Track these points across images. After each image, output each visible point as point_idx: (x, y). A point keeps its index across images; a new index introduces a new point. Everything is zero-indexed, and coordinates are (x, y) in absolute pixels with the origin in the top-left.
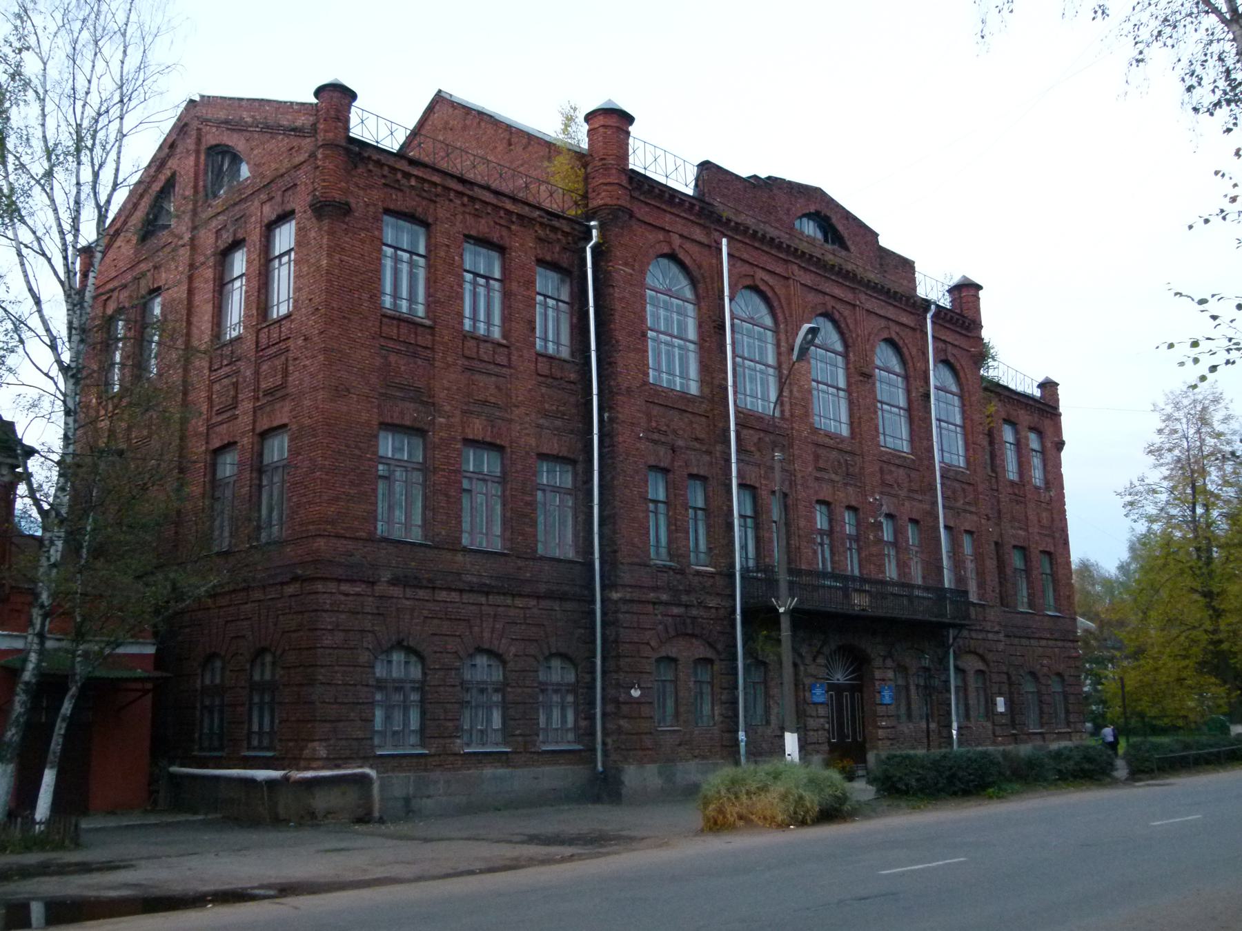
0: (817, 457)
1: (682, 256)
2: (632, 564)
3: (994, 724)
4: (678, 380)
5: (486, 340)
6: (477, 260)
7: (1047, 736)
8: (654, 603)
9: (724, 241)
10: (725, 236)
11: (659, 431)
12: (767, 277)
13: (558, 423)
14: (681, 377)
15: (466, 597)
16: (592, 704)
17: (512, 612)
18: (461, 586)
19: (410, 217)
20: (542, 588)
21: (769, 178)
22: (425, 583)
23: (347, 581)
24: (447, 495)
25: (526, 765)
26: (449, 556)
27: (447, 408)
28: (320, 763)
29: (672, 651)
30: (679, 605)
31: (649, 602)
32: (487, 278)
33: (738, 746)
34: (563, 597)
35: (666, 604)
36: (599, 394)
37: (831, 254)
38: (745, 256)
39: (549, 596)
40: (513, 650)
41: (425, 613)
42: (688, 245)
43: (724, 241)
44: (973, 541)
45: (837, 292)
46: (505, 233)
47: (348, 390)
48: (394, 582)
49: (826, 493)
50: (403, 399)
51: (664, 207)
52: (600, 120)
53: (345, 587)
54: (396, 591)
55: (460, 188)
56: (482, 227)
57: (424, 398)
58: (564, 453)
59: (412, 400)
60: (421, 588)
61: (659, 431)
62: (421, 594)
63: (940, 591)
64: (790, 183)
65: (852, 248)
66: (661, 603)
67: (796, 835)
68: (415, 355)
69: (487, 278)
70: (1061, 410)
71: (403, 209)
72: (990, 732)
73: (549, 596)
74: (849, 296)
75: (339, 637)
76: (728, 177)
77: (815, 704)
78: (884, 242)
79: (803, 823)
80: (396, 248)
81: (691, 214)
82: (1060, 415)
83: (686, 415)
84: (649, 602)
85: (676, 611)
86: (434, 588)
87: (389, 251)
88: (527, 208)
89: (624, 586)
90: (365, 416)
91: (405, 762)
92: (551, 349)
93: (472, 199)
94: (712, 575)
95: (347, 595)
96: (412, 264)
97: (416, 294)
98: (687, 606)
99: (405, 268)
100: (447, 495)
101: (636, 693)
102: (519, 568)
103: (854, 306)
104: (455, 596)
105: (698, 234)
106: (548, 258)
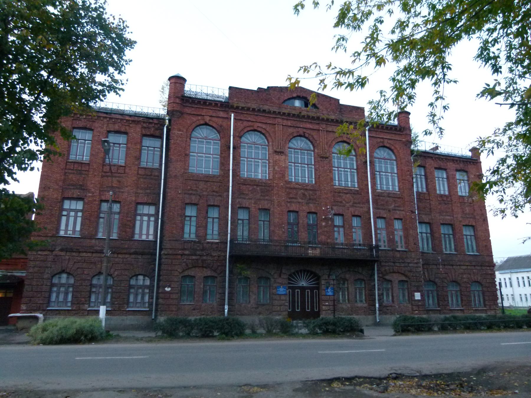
0: (289, 193)
1: (211, 123)
2: (170, 240)
3: (412, 305)
4: (343, 182)
5: (445, 196)
6: (458, 175)
7: (465, 311)
8: (182, 255)
9: (233, 115)
10: (233, 112)
11: (192, 190)
12: (260, 125)
13: (148, 191)
14: (345, 181)
15: (94, 255)
16: (153, 293)
17: (117, 260)
18: (92, 251)
19: (85, 128)
20: (132, 251)
21: (268, 87)
22: (74, 250)
23: (85, 252)
24: (90, 220)
25: (118, 315)
26: (88, 241)
27: (93, 190)
28: (23, 312)
29: (191, 273)
30: (196, 255)
31: (179, 255)
32: (463, 180)
33: (224, 311)
34: (142, 254)
35: (188, 255)
36: (164, 179)
37: (310, 111)
38: (249, 119)
39: (136, 253)
40: (116, 273)
41: (75, 260)
42: (214, 119)
43: (233, 115)
44: (402, 222)
45: (311, 126)
46: (127, 128)
47: (49, 188)
48: (62, 250)
49: (293, 207)
50: (73, 189)
51: (202, 107)
52: (173, 81)
53: (39, 253)
54: (63, 253)
55: (105, 115)
56: (458, 167)
57: (83, 188)
58: (150, 201)
59: (77, 188)
60: (74, 252)
61: (192, 190)
62: (74, 254)
63: (371, 248)
64: (281, 87)
65: (321, 107)
66: (185, 255)
67: (42, 347)
68: (81, 174)
69: (463, 180)
70: (481, 160)
71: (81, 126)
72: (410, 309)
73: (136, 253)
74: (316, 127)
75: (36, 269)
76: (237, 91)
77: (279, 294)
78: (341, 102)
79: (44, 344)
80: (380, 172)
81: (218, 107)
82: (481, 162)
83: (208, 183)
84: (179, 255)
85: (194, 257)
86: (80, 252)
87: (378, 173)
88: (136, 118)
89: (166, 249)
90: (55, 196)
91: (61, 312)
92: (442, 193)
93: (111, 118)
94: (217, 243)
95: (42, 255)
96: (421, 178)
97: (395, 184)
98: (200, 256)
99: (419, 179)
100: (90, 220)
101: (168, 289)
102: (122, 244)
103: (319, 130)
104: (89, 255)
105: (222, 114)
106: (149, 133)
